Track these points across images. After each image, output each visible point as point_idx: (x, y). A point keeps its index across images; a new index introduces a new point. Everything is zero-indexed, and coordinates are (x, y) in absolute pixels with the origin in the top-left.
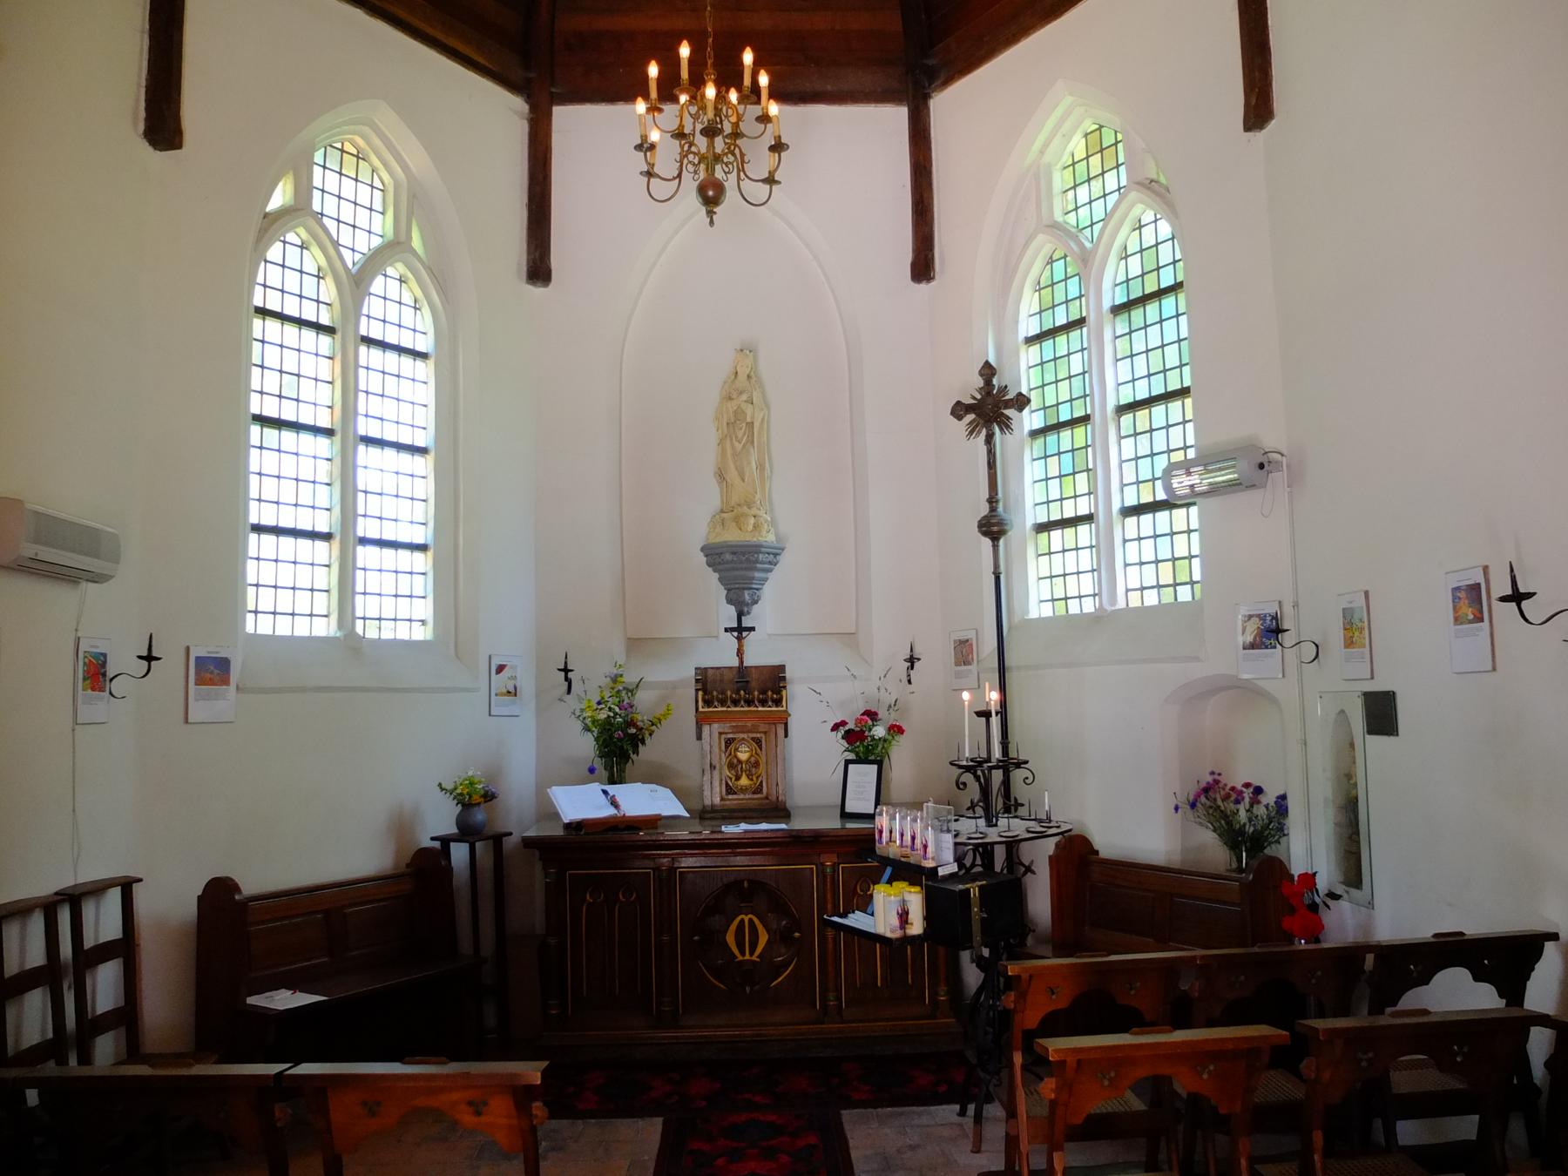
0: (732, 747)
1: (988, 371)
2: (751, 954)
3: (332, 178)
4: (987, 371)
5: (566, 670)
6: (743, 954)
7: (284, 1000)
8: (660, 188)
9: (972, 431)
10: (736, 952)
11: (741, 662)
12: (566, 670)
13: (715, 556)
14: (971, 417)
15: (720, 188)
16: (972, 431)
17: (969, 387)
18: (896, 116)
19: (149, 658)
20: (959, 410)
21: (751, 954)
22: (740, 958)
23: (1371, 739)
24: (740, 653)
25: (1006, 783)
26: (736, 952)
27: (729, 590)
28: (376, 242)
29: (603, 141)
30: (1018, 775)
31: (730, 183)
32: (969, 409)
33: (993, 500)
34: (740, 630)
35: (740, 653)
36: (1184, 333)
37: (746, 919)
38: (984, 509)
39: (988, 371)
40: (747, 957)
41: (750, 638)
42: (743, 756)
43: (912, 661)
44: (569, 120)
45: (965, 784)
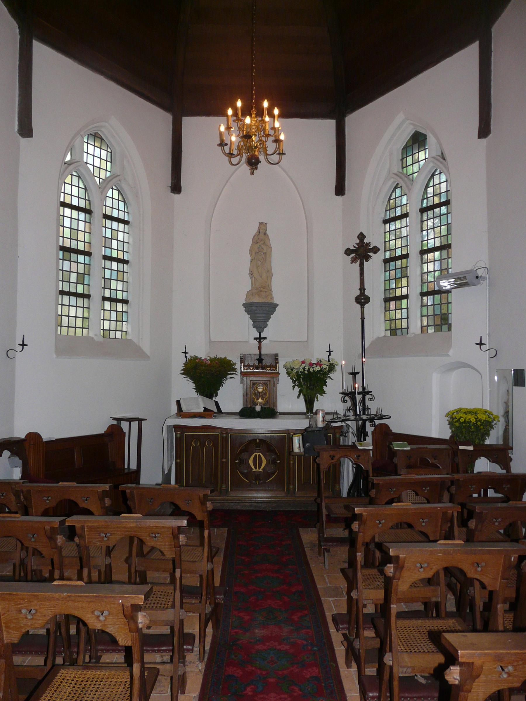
0: (256, 386)
1: (361, 236)
2: (259, 469)
3: (91, 148)
4: (360, 236)
5: (185, 353)
6: (256, 468)
7: (496, 378)
8: (235, 160)
9: (353, 261)
10: (253, 467)
11: (260, 352)
12: (185, 353)
13: (248, 307)
14: (353, 255)
15: (258, 161)
16: (353, 261)
17: (353, 243)
18: (330, 124)
19: (23, 345)
20: (348, 252)
21: (259, 469)
22: (255, 470)
23: (514, 387)
24: (260, 348)
25: (363, 401)
26: (253, 467)
27: (254, 322)
28: (108, 174)
29: (204, 133)
30: (367, 397)
31: (261, 158)
32: (352, 251)
33: (362, 289)
34: (260, 339)
35: (260, 348)
36: (427, 156)
37: (258, 454)
38: (358, 293)
39: (361, 236)
40: (258, 470)
41: (264, 342)
42: (260, 390)
43: (330, 351)
44: (191, 124)
45: (347, 401)
